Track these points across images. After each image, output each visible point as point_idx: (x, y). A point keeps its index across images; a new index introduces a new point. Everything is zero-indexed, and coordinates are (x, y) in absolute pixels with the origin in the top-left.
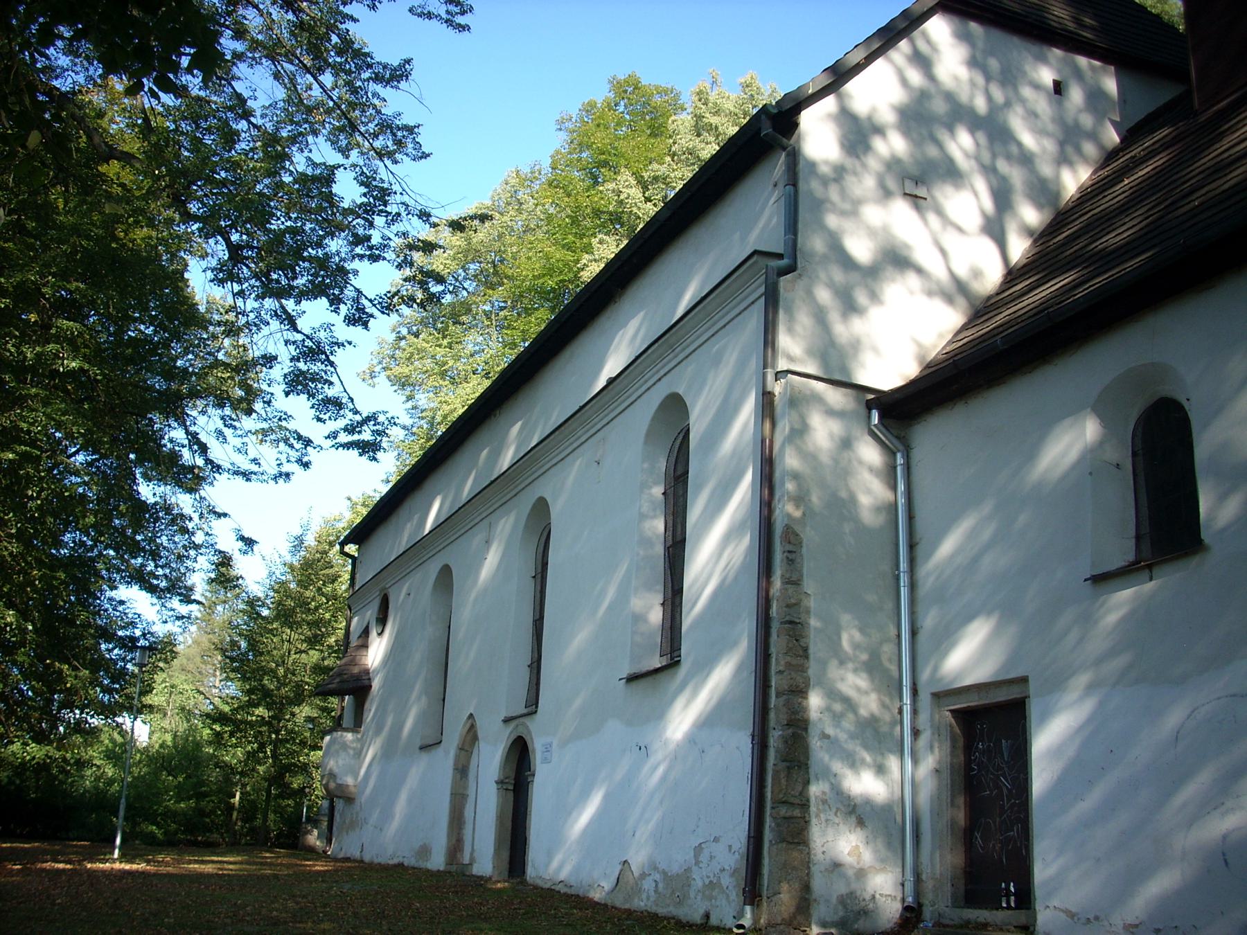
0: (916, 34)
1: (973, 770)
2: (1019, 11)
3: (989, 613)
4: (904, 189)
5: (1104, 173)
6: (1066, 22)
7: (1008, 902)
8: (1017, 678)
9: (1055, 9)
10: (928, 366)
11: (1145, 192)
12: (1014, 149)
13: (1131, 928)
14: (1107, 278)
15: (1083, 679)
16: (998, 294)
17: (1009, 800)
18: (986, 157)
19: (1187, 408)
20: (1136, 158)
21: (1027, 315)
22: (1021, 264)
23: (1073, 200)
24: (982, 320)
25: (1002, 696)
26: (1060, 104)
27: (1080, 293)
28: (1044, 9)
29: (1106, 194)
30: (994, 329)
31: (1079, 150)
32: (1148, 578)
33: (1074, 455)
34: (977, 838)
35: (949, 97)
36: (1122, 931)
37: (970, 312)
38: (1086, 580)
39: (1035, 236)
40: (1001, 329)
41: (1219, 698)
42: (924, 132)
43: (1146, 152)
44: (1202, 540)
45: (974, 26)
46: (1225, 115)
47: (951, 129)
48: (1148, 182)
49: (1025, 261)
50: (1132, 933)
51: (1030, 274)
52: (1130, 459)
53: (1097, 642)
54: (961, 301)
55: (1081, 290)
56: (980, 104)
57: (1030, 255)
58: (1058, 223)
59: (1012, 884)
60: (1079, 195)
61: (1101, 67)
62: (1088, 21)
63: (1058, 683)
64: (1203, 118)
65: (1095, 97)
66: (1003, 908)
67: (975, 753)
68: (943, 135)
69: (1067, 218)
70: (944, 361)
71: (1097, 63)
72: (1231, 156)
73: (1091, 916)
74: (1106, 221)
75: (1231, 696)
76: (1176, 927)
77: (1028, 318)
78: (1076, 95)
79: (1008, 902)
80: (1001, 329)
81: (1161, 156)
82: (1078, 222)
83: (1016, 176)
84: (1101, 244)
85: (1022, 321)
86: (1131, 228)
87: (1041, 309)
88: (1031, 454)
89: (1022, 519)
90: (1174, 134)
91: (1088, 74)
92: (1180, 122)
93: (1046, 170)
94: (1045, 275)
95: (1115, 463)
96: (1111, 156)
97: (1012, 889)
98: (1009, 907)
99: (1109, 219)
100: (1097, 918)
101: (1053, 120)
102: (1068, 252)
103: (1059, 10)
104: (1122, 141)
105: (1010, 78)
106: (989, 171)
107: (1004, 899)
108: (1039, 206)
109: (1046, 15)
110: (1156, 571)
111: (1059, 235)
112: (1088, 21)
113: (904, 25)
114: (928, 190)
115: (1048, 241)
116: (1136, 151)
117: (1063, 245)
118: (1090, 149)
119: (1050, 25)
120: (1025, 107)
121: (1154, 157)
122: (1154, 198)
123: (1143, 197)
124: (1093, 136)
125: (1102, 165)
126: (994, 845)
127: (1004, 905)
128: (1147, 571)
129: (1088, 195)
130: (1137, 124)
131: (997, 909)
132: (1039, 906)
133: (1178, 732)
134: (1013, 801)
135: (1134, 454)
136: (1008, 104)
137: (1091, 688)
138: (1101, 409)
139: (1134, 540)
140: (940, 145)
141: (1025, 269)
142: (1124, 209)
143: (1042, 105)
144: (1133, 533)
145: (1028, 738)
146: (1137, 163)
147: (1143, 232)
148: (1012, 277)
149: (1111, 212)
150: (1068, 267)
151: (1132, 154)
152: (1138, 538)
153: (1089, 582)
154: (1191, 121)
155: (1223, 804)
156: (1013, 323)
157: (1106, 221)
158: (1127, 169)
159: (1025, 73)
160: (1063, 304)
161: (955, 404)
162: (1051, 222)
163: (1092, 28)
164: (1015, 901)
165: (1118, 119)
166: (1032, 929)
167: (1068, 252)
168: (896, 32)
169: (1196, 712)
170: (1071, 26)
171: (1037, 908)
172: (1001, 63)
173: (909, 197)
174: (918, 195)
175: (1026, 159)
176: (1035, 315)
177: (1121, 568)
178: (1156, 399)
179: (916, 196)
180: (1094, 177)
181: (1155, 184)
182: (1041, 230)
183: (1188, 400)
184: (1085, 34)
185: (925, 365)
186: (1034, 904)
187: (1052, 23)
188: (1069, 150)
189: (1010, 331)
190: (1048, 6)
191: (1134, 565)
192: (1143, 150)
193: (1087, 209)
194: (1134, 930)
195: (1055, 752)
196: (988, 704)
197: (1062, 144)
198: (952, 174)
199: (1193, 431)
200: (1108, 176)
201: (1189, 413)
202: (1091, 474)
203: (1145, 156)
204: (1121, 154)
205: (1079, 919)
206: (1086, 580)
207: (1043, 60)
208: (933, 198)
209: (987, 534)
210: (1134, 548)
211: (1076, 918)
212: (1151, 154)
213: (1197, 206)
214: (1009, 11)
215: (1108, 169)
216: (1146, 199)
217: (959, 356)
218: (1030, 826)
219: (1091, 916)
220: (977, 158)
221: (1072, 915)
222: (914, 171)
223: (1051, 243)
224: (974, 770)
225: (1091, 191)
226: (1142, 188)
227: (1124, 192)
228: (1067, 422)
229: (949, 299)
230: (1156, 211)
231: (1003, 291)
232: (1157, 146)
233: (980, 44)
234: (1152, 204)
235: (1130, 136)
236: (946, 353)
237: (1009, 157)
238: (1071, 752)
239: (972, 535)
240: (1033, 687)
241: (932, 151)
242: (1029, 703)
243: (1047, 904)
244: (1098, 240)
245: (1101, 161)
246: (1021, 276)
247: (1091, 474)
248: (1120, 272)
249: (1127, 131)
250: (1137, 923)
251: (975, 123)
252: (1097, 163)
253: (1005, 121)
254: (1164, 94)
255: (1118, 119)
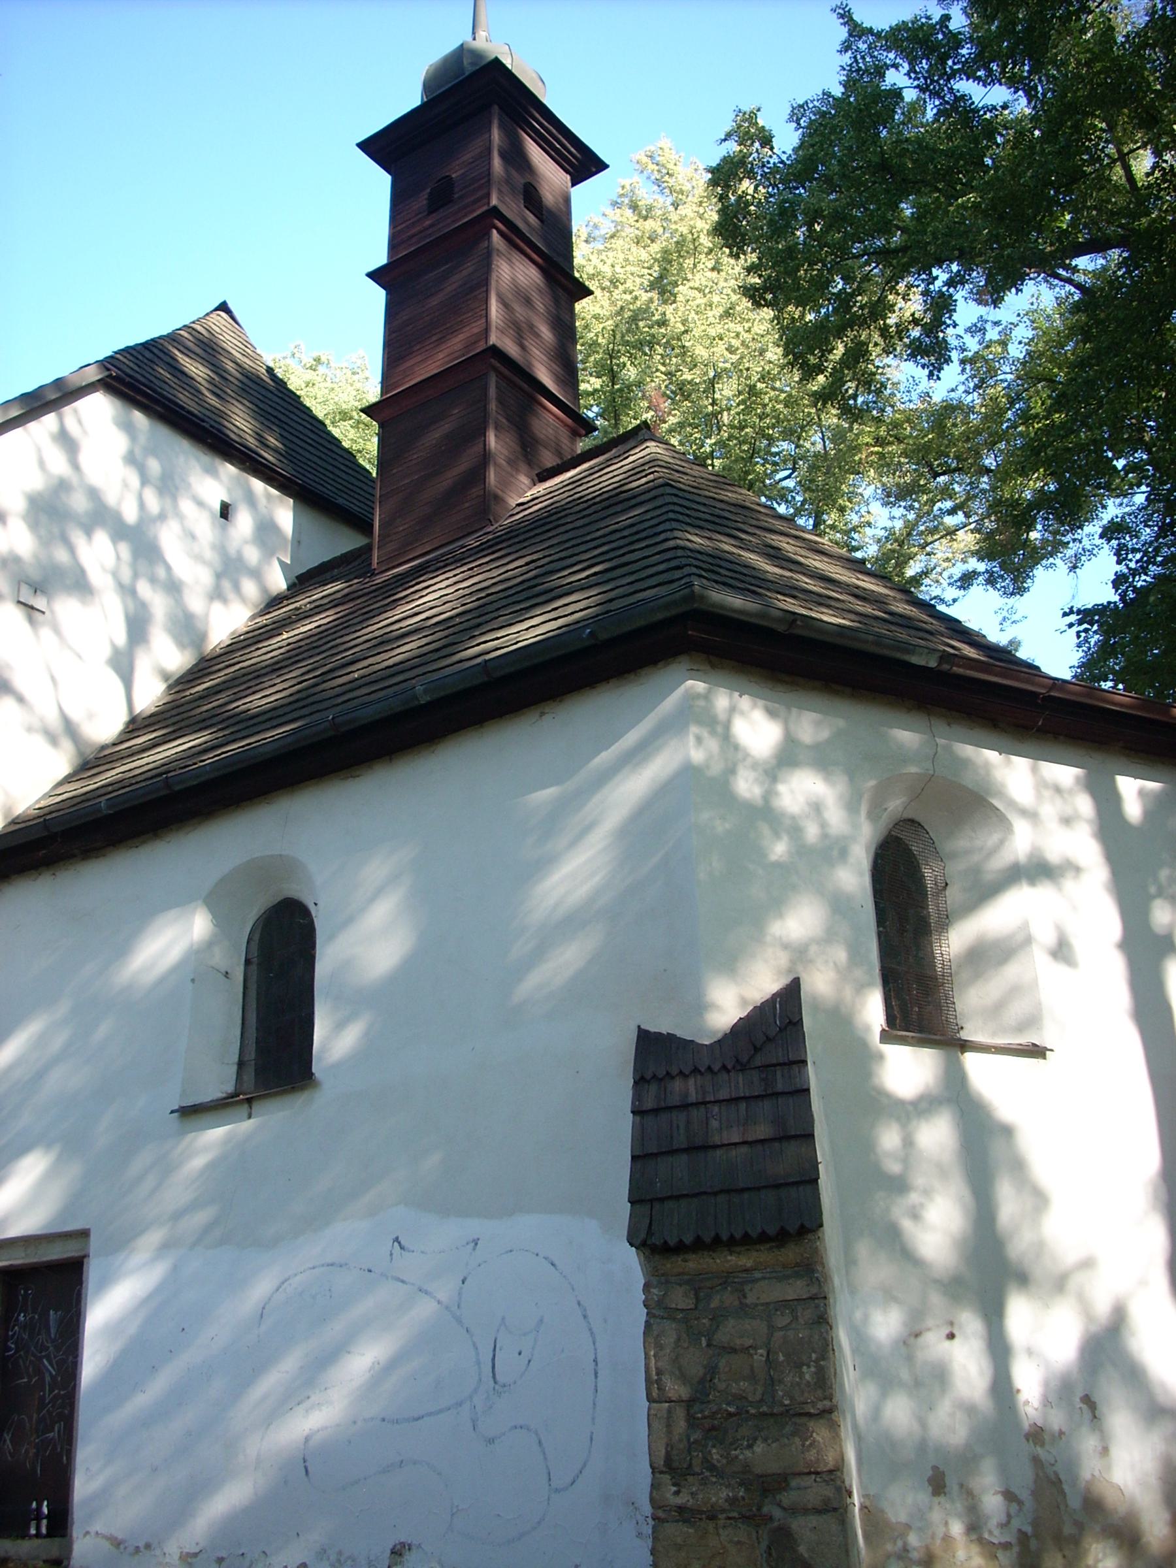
0: (67, 410)
1: (10, 1349)
2: (196, 412)
3: (49, 1146)
4: (18, 596)
5: (262, 620)
6: (248, 437)
7: (38, 1528)
8: (78, 1231)
9: (237, 418)
10: (14, 822)
11: (303, 653)
12: (161, 573)
13: (188, 1558)
14: (243, 747)
15: (153, 1238)
16: (114, 744)
17: (51, 1391)
18: (126, 574)
19: (314, 914)
20: (301, 611)
21: (143, 777)
22: (149, 713)
23: (222, 646)
24: (89, 774)
25: (55, 1253)
26: (224, 529)
27: (210, 758)
28: (225, 416)
29: (260, 646)
30: (103, 787)
31: (237, 588)
32: (246, 1115)
33: (175, 954)
34: (5, 1441)
35: (94, 494)
36: (177, 1562)
37: (77, 761)
38: (172, 1112)
39: (170, 682)
40: (110, 788)
41: (314, 1268)
42: (56, 530)
43: (313, 605)
44: (312, 1074)
45: (139, 417)
46: (404, 581)
47: (89, 532)
48: (308, 641)
49: (153, 710)
50: (190, 1564)
51: (156, 727)
52: (242, 968)
53: (177, 1193)
54: (67, 746)
55: (211, 756)
56: (130, 514)
57: (160, 704)
58: (199, 671)
59: (45, 1503)
60: (230, 642)
61: (278, 496)
62: (272, 441)
63: (123, 1242)
64: (380, 579)
65: (265, 530)
66: (31, 1537)
67: (14, 1327)
68: (79, 539)
69: (210, 667)
70: (34, 819)
71: (274, 492)
72: (401, 628)
73: (141, 1544)
74: (254, 678)
75: (328, 1265)
76: (243, 1554)
77: (144, 780)
78: (244, 522)
79: (38, 1528)
80: (110, 788)
81: (327, 613)
82: (222, 673)
83: (158, 604)
84: (244, 704)
85: (137, 783)
86: (280, 691)
87: (162, 772)
88: (123, 949)
89: (103, 1030)
90: (346, 591)
91: (262, 501)
92: (356, 578)
93: (195, 603)
94: (174, 731)
95: (223, 971)
96: (275, 602)
97: (45, 1510)
98: (38, 1535)
99: (259, 676)
100: (148, 1546)
101: (214, 547)
102: (205, 708)
103: (243, 422)
104: (288, 589)
105: (169, 486)
106: (128, 591)
107: (33, 1524)
108: (181, 645)
109: (226, 423)
110: (256, 1107)
111: (199, 684)
112: (272, 441)
113: (53, 397)
114: (48, 602)
115: (184, 690)
116: (303, 602)
117: (201, 698)
118: (250, 588)
119: (228, 436)
120: (182, 524)
121: (320, 613)
122: (312, 661)
123: (300, 657)
124: (256, 574)
125: (261, 611)
126: (27, 1451)
127: (33, 1531)
128: (246, 1106)
129: (241, 644)
130: (308, 571)
131: (23, 1537)
132: (76, 1531)
133: (264, 1308)
134: (56, 1391)
135: (248, 962)
136: (162, 517)
137: (165, 1247)
138: (214, 902)
139: (235, 1068)
140: (72, 550)
141: (152, 719)
142: (276, 668)
143: (204, 525)
144: (236, 1058)
145: (82, 1309)
146: (302, 616)
147: (291, 699)
148: (135, 726)
149: (263, 668)
150: (202, 725)
151: (297, 605)
152: (241, 1064)
153: (176, 1114)
154: (367, 580)
155: (308, 1398)
156: (126, 783)
157: (255, 677)
158: (288, 621)
159: (189, 485)
160: (187, 769)
161: (542, 714)
162: (191, 669)
163: (275, 450)
164: (48, 1528)
165: (289, 562)
166: (65, 1563)
167: (205, 708)
168: (43, 401)
169: (285, 1284)
170: (252, 442)
171: (75, 1534)
172: (162, 466)
173: (22, 607)
174: (35, 606)
175: (173, 587)
176: (152, 778)
177: (217, 1100)
178: (279, 899)
179: (32, 608)
180: (250, 624)
181: (315, 645)
182: (181, 672)
183: (316, 904)
184: (266, 455)
185: (9, 820)
186: (72, 1530)
187: (228, 432)
188: (226, 585)
189: (120, 792)
190: (230, 413)
191: (232, 1097)
192: (310, 603)
193: (236, 660)
194: (194, 1560)
195: (112, 1329)
196: (36, 1263)
197: (219, 576)
198: (80, 585)
199: (318, 941)
200: (267, 625)
201: (315, 919)
202: (193, 980)
203: (311, 609)
204: (285, 602)
205: (125, 1548)
206: (172, 1112)
207: (212, 472)
208: (52, 612)
209: (58, 1043)
210: (234, 1077)
211: (122, 1547)
212: (318, 609)
213: (357, 679)
214: (183, 408)
215: (267, 617)
216: (304, 659)
217: (54, 815)
218: (75, 1425)
219: (141, 1544)
220: (115, 574)
221: (117, 1543)
222: (35, 574)
223: (188, 693)
224: (10, 1349)
225: (244, 640)
226: (300, 647)
227: (280, 648)
228: (172, 914)
229: (53, 740)
230: (311, 676)
231: (122, 742)
232: (326, 601)
233: (142, 439)
234: (309, 667)
235: (301, 582)
236: (39, 809)
237: (153, 580)
238: (132, 1329)
239: (40, 1041)
240: (94, 1242)
241: (61, 555)
242: (88, 1263)
243: (88, 1529)
244: (241, 698)
245: (262, 606)
246: (146, 726)
247: (193, 980)
248: (259, 741)
249: (297, 577)
250: (197, 1551)
251: (120, 531)
252: (256, 606)
253: (156, 538)
254: (345, 542)
255: (289, 562)
